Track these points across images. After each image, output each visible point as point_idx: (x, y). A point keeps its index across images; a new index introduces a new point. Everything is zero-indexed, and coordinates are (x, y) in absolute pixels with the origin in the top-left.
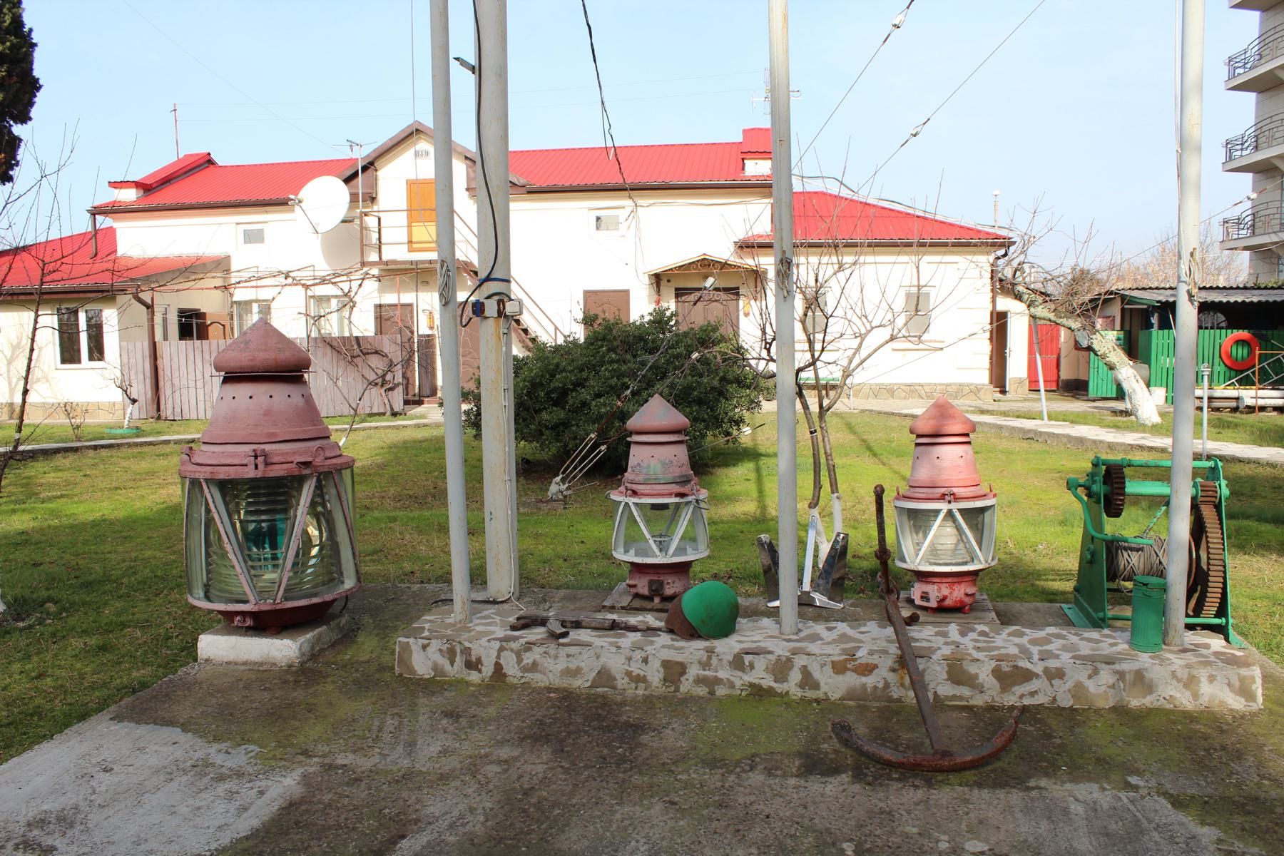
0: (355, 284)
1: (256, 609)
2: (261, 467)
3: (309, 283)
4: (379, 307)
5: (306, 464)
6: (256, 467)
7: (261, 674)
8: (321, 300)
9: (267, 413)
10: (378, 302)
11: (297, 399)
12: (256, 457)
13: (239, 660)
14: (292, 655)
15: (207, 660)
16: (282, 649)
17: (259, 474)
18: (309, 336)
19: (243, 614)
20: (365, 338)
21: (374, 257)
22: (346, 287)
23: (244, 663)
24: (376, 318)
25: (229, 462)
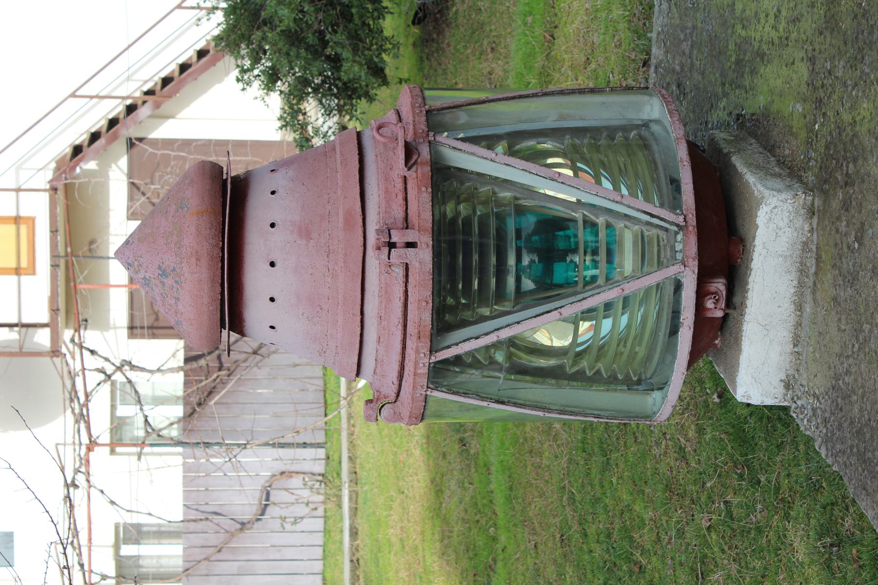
0: (91, 362)
1: (694, 265)
2: (411, 236)
3: (85, 440)
4: (134, 330)
5: (410, 151)
6: (411, 245)
7: (826, 266)
8: (118, 425)
9: (305, 232)
10: (125, 332)
11: (279, 181)
12: (392, 245)
13: (792, 320)
14: (788, 206)
15: (788, 386)
16: (775, 224)
17: (425, 240)
18: (179, 443)
19: (701, 294)
20: (187, 348)
21: (43, 338)
22: (93, 378)
23: (799, 307)
24: (154, 336)
25: (398, 305)
